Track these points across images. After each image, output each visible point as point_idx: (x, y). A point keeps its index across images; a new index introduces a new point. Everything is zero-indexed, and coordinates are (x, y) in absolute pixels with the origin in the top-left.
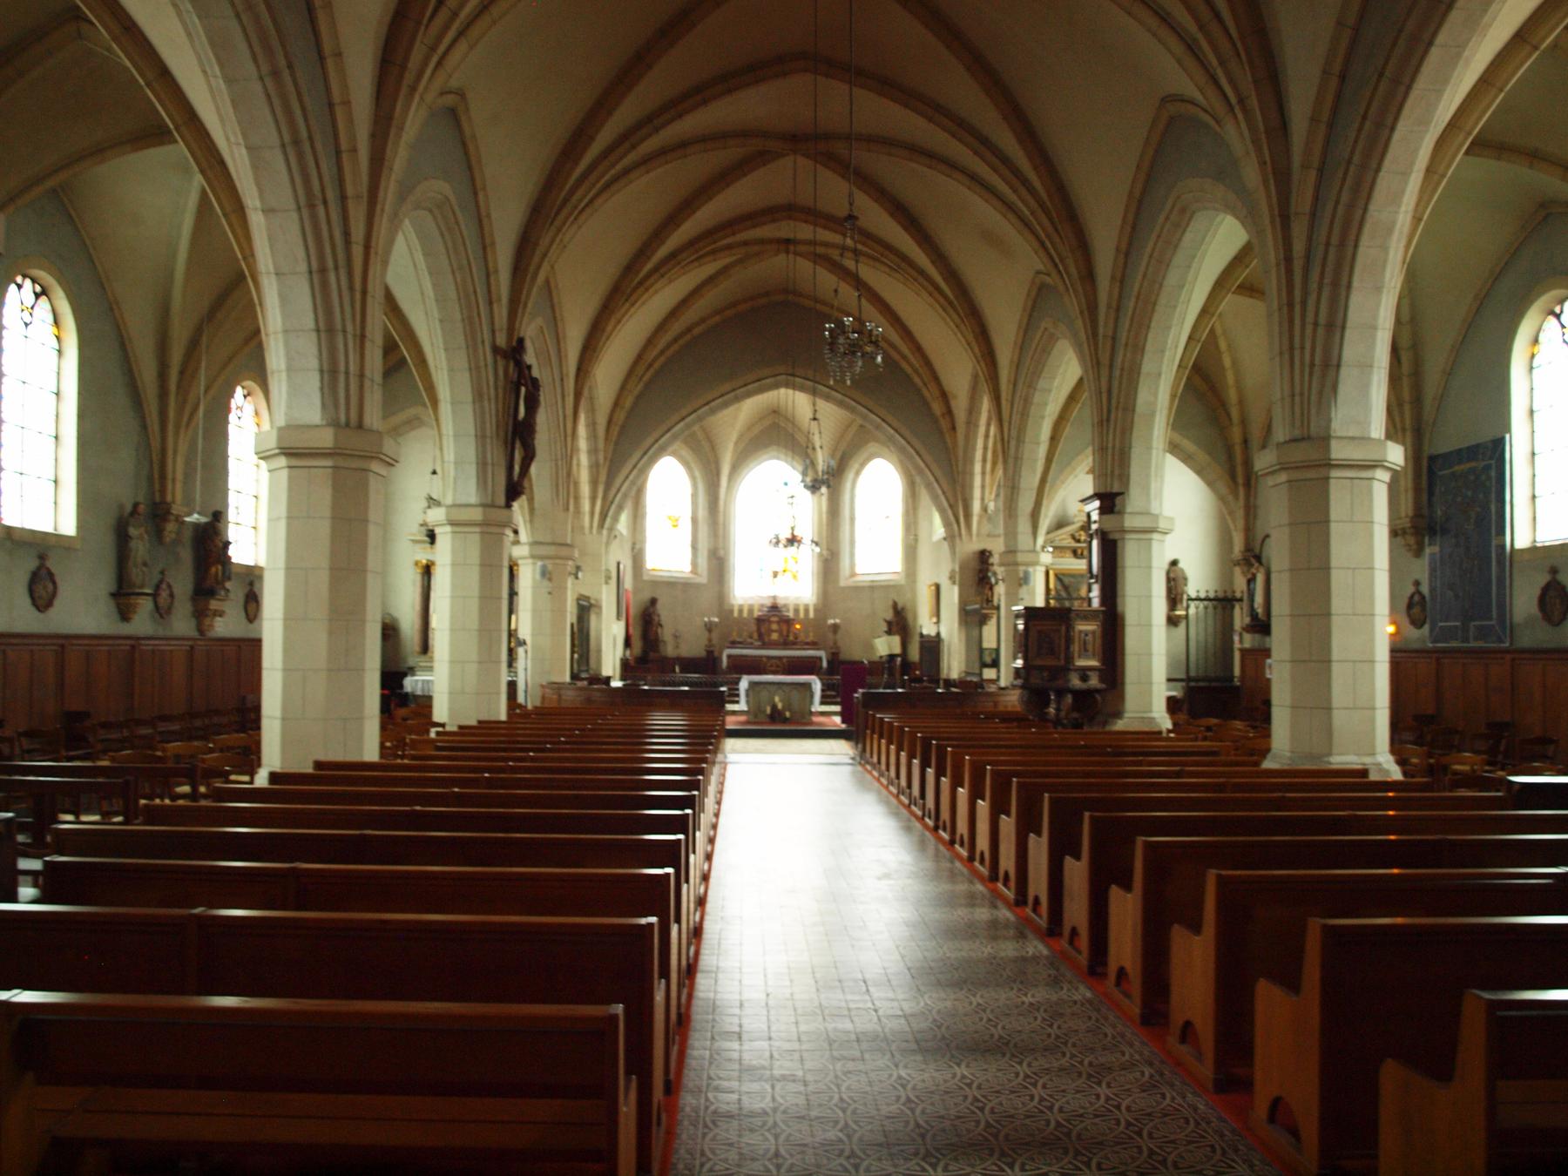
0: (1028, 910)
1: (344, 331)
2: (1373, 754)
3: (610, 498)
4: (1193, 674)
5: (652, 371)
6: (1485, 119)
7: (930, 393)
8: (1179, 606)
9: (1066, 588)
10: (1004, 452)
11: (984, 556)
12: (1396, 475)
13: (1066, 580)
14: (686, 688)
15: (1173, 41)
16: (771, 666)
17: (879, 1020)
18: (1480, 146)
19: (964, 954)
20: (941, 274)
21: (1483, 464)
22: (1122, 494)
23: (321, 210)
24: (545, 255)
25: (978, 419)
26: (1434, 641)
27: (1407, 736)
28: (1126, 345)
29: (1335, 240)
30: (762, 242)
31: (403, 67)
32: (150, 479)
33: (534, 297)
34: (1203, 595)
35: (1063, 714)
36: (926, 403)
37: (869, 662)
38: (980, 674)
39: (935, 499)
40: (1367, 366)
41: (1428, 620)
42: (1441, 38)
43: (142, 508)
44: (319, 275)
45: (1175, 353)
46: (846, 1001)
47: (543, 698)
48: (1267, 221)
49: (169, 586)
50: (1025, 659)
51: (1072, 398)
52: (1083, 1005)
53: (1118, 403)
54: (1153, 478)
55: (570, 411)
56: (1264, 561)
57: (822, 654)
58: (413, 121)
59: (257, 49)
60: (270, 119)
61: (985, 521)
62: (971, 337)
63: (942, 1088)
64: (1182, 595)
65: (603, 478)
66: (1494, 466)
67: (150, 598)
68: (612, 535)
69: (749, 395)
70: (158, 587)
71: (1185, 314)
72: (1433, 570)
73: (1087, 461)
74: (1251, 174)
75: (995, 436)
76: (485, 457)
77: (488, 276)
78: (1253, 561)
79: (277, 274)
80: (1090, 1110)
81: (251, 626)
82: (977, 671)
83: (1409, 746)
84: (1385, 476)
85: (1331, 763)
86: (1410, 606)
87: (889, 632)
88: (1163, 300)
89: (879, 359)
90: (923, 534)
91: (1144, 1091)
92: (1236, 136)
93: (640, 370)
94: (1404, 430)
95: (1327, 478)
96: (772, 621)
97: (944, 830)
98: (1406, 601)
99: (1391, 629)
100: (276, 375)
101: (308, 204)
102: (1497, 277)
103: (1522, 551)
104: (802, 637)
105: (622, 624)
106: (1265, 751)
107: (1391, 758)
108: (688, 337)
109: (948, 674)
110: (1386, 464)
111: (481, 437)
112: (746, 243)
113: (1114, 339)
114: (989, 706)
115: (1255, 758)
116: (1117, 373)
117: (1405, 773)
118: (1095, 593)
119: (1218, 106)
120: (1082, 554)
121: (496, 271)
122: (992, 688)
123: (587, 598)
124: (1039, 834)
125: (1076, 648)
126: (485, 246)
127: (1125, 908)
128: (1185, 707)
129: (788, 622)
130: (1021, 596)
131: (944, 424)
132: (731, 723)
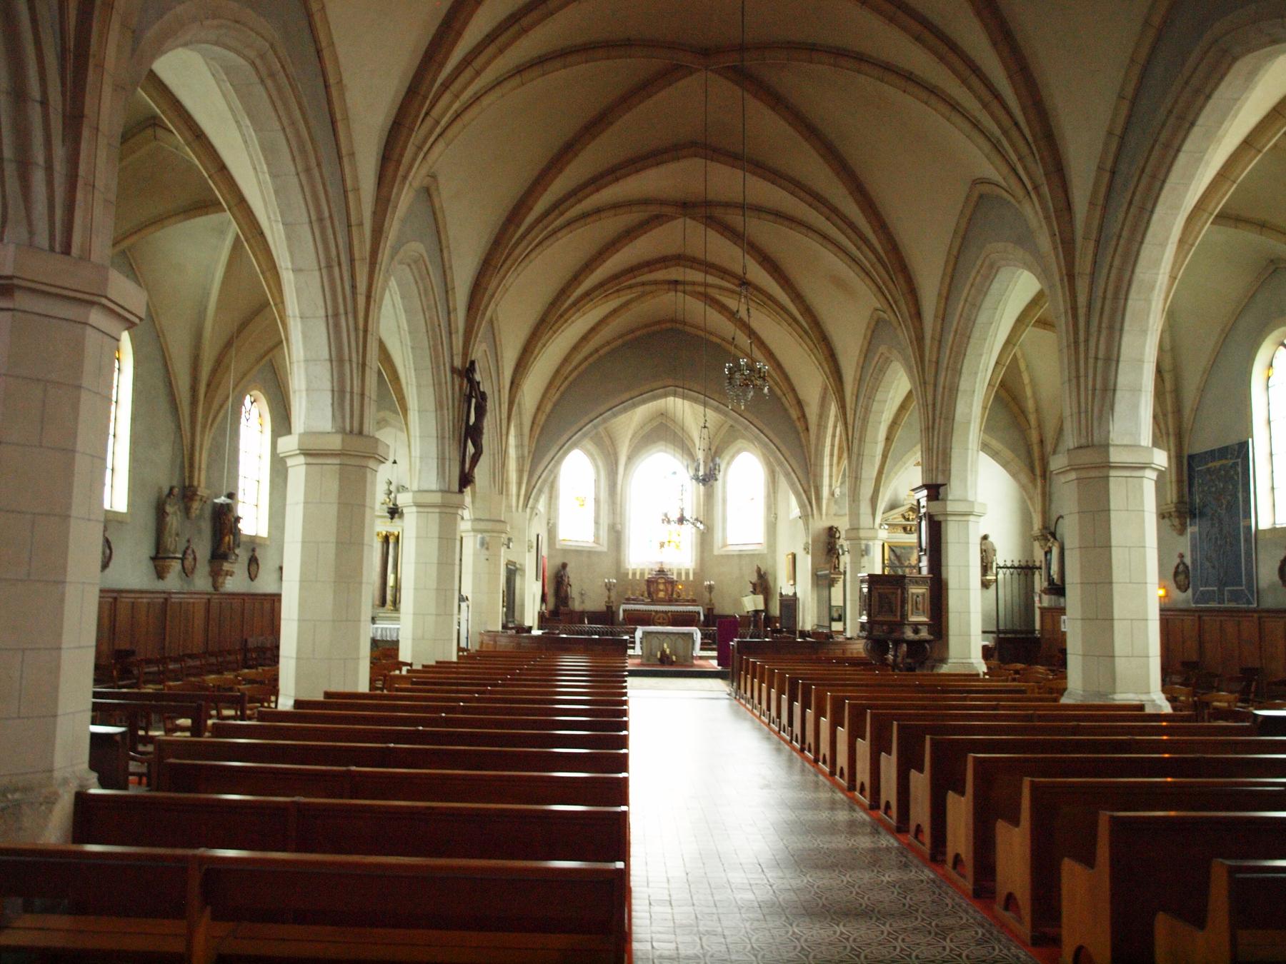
0: (881, 813)
1: (350, 361)
2: (1148, 693)
3: (533, 483)
4: (1001, 628)
5: (566, 383)
6: (1227, 197)
7: (788, 401)
8: (989, 573)
9: (898, 557)
10: (848, 450)
11: (832, 532)
12: (1161, 474)
13: (898, 551)
14: (597, 637)
15: (981, 140)
17: (774, 892)
18: (1224, 218)
19: (834, 845)
20: (798, 310)
21: (1231, 462)
22: (945, 485)
23: (336, 270)
24: (493, 296)
25: (827, 423)
26: (1196, 602)
27: (1176, 678)
28: (947, 368)
29: (1109, 295)
30: (656, 283)
31: (399, 163)
32: (182, 468)
33: (483, 328)
34: (1009, 564)
35: (899, 659)
36: (786, 410)
37: (740, 616)
38: (830, 627)
39: (792, 485)
40: (1136, 390)
41: (1191, 585)
42: (1187, 147)
43: (176, 491)
44: (333, 319)
45: (986, 376)
46: (748, 879)
47: (482, 643)
48: (1057, 278)
49: (193, 552)
50: (869, 615)
51: (903, 407)
52: (928, 883)
53: (941, 414)
54: (969, 472)
55: (504, 416)
56: (1058, 536)
57: (700, 609)
58: (405, 199)
59: (296, 153)
60: (302, 202)
61: (832, 503)
62: (822, 358)
63: (827, 941)
64: (992, 563)
65: (527, 467)
66: (1240, 464)
67: (180, 561)
68: (534, 513)
69: (644, 402)
70: (185, 553)
71: (993, 344)
72: (1193, 550)
73: (917, 455)
74: (1044, 241)
75: (841, 435)
76: (443, 453)
77: (449, 313)
78: (1049, 537)
79: (301, 318)
80: (938, 958)
81: (253, 583)
82: (827, 624)
83: (1177, 686)
84: (1152, 475)
85: (1114, 700)
86: (1176, 574)
87: (754, 592)
88: (976, 334)
89: (766, 390)
90: (781, 514)
91: (980, 944)
92: (1032, 213)
93: (557, 383)
94: (1168, 434)
95: (1108, 477)
96: (659, 584)
97: (810, 751)
98: (1172, 571)
99: (1162, 592)
100: (297, 394)
101: (328, 265)
102: (1239, 315)
103: (1264, 531)
104: (683, 596)
105: (540, 583)
106: (1062, 691)
107: (1163, 696)
108: (596, 356)
109: (803, 626)
110: (1153, 466)
111: (441, 438)
112: (643, 284)
113: (937, 363)
114: (839, 653)
115: (1054, 695)
116: (940, 389)
117: (1174, 708)
118: (924, 563)
119: (1020, 192)
120: (911, 530)
121: (455, 309)
122: (840, 638)
123: (514, 564)
124: (889, 753)
125: (909, 607)
126: (447, 290)
127: (960, 809)
128: (996, 654)
129: (672, 583)
130: (862, 565)
131: (800, 426)
132: (631, 664)
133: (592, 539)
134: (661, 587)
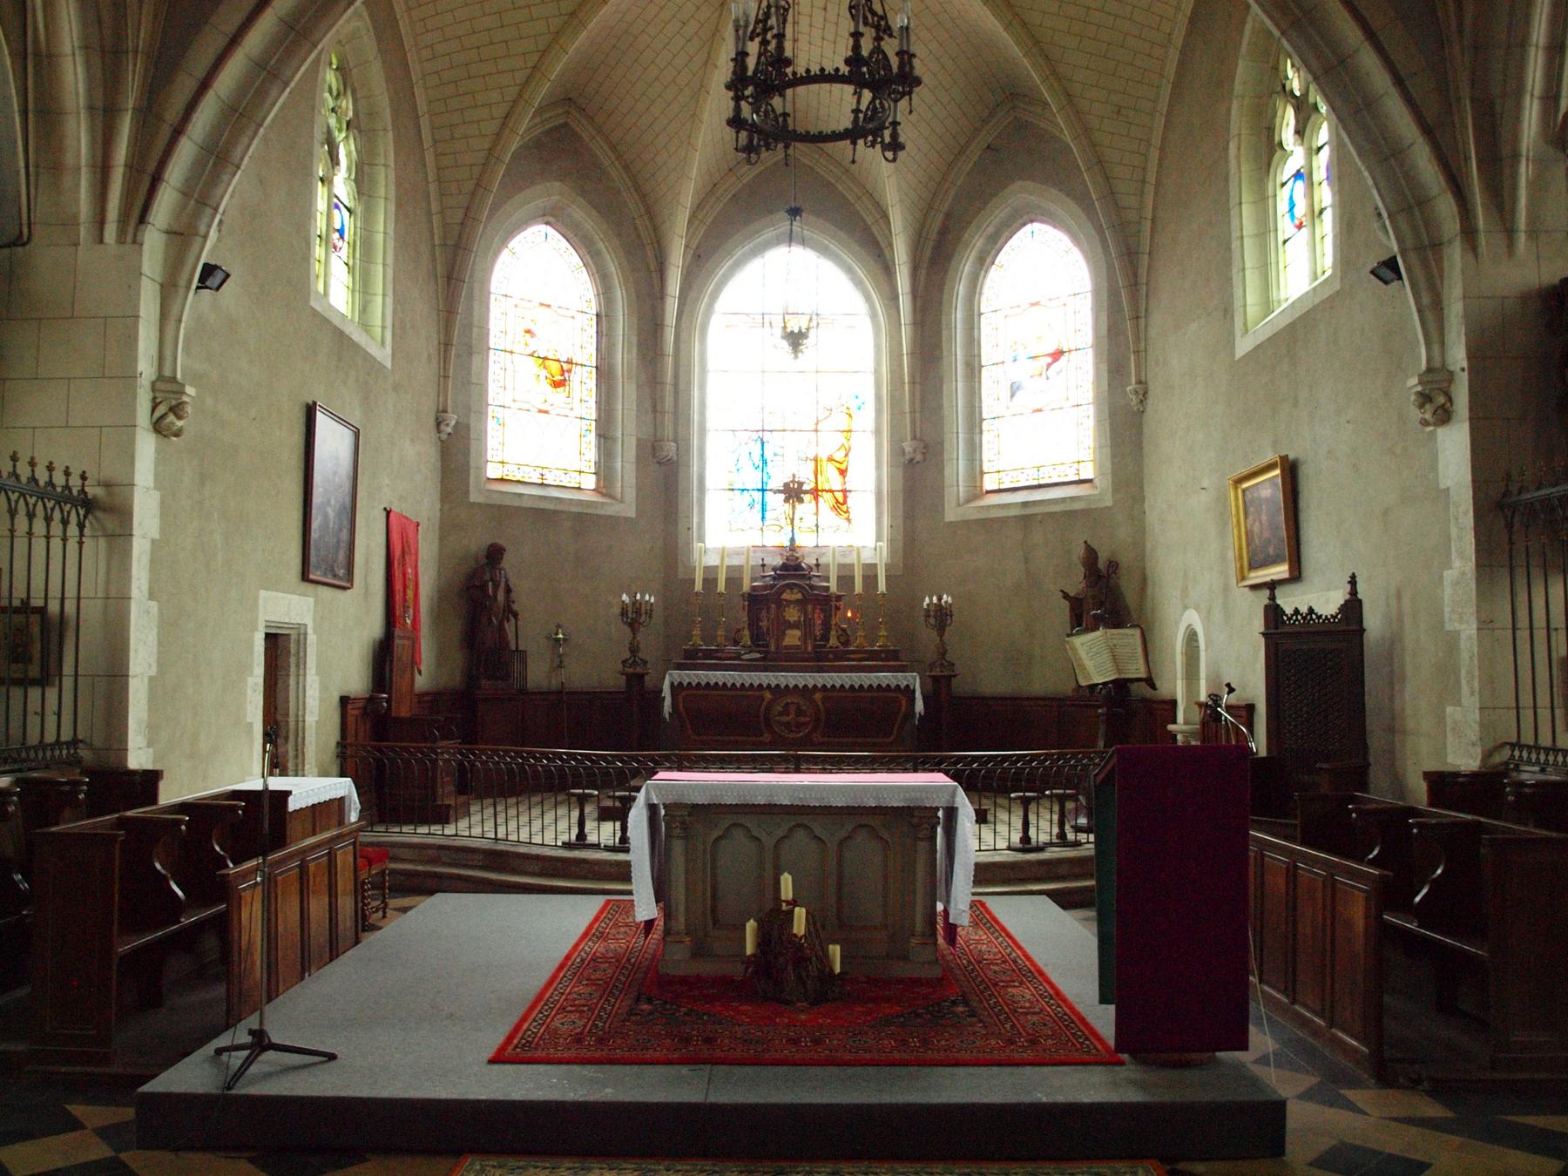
3: (172, 115)
133: (589, 482)
134: (792, 614)
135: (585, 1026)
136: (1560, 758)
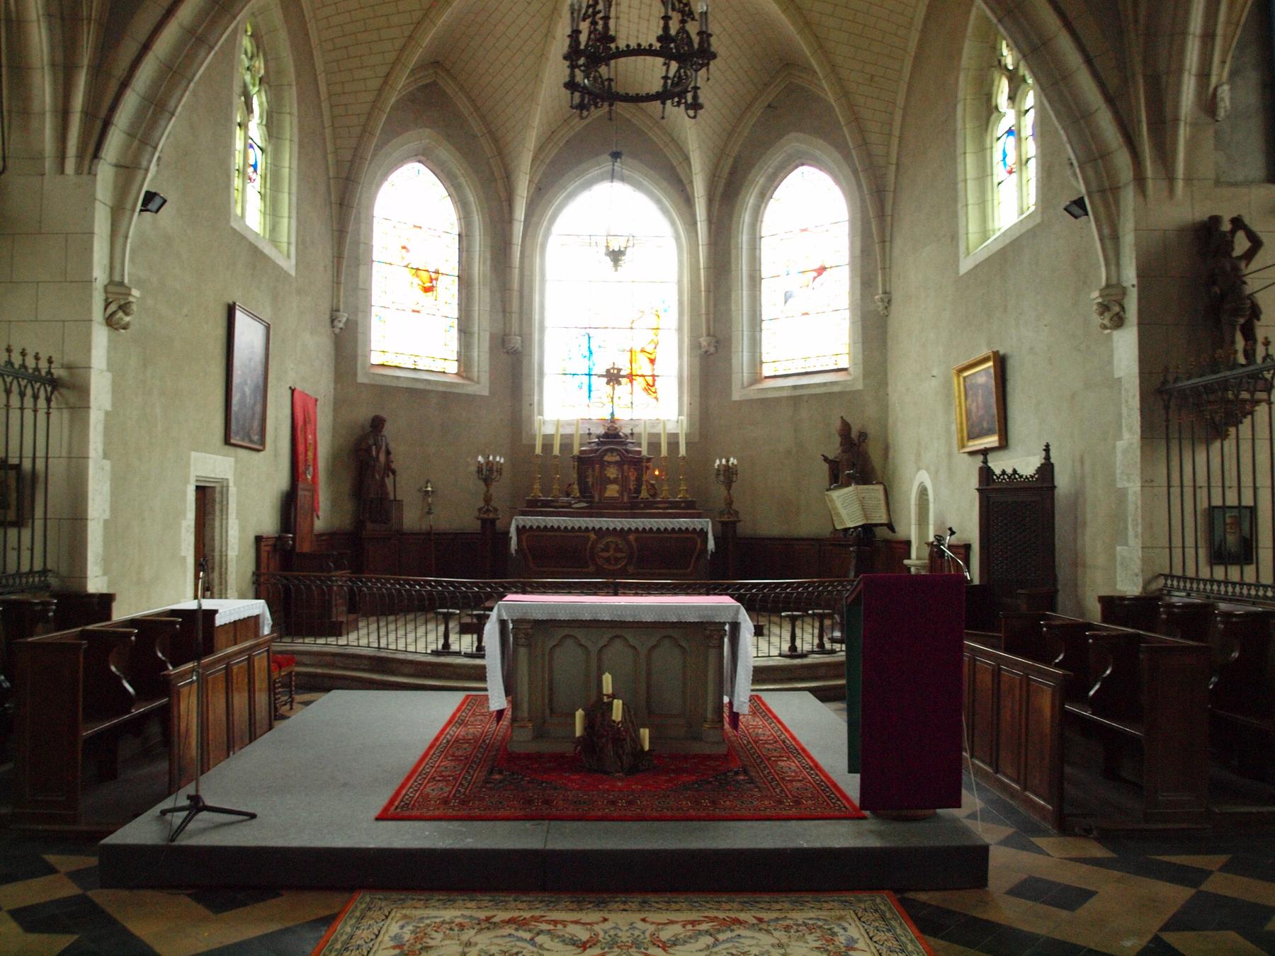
16: (606, 549)
104: (664, 493)
129: (638, 463)
133: (452, 368)
134: (612, 473)
135: (450, 792)
136: (1270, 594)
